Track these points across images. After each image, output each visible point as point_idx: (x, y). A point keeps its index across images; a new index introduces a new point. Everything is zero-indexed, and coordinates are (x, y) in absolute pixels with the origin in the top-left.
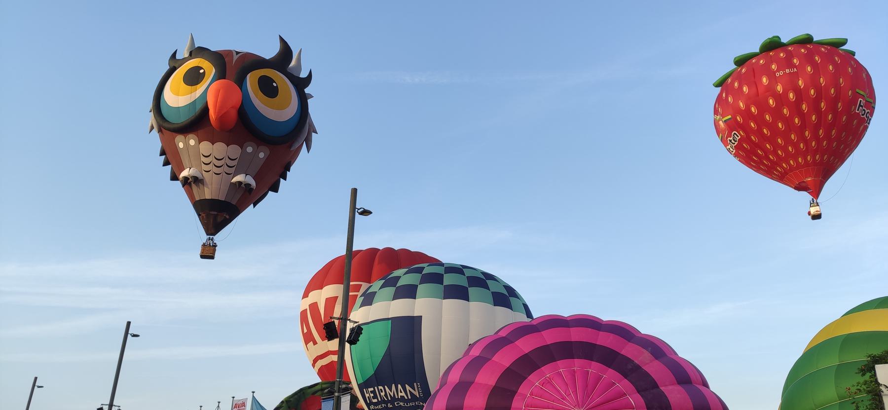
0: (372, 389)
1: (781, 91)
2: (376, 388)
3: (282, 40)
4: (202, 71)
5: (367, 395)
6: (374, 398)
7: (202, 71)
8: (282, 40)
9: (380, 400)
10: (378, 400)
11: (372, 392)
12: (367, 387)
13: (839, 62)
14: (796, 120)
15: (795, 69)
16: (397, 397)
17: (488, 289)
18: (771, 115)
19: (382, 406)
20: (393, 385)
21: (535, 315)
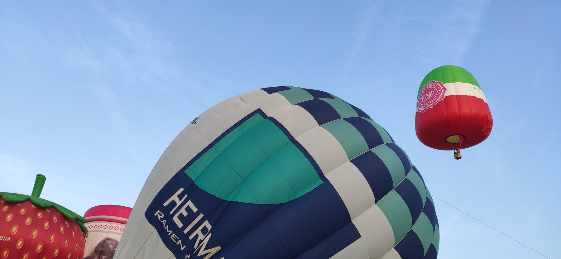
0: (195, 210)
1: (35, 237)
2: (201, 216)
6: (181, 217)
9: (186, 232)
11: (188, 209)
13: (55, 222)
15: (9, 238)
17: (345, 119)
19: (177, 240)
20: (218, 248)
21: (42, 196)
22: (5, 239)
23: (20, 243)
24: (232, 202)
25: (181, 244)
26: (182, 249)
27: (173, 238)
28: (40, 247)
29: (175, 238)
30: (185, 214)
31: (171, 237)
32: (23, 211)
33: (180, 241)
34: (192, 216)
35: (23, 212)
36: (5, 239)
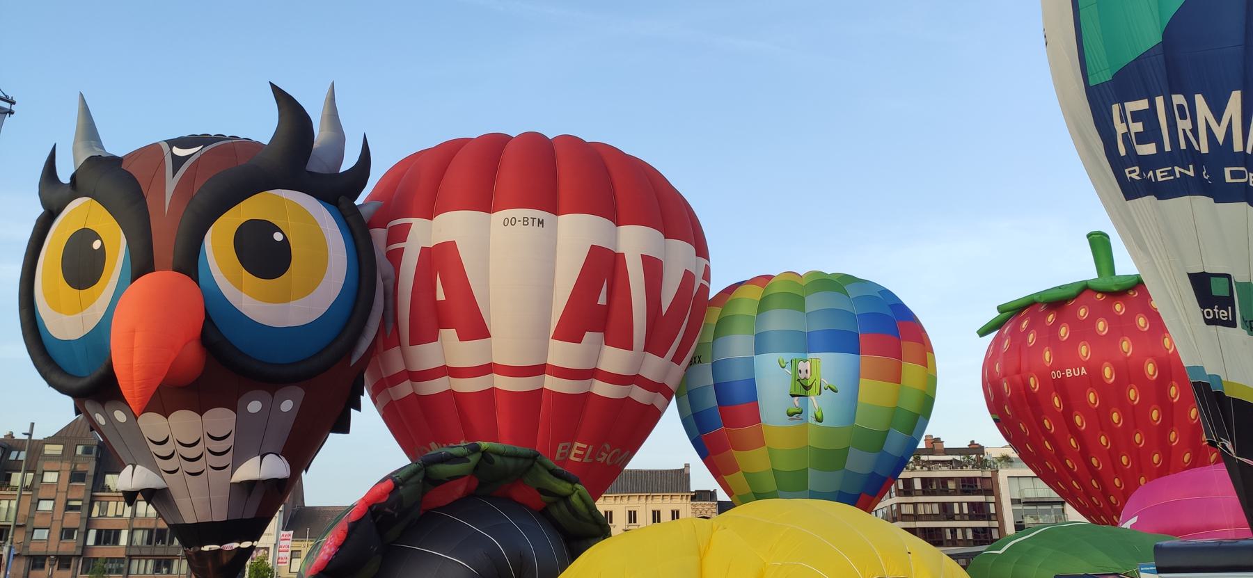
0: (1143, 105)
2: (1160, 101)
3: (278, 93)
4: (96, 245)
5: (1120, 128)
6: (1142, 138)
7: (96, 245)
8: (278, 93)
9: (1168, 148)
10: (1160, 146)
11: (1137, 116)
12: (1122, 99)
14: (1156, 458)
15: (1083, 368)
16: (1238, 147)
18: (1142, 392)
19: (1172, 173)
22: (1077, 373)
23: (1107, 372)
24: (1167, 34)
25: (1182, 170)
26: (1191, 173)
27: (1162, 177)
28: (1150, 369)
29: (1166, 174)
30: (1138, 127)
31: (1159, 180)
32: (1082, 312)
33: (1177, 169)
34: (1148, 117)
35: (1085, 315)
36: (1077, 373)
